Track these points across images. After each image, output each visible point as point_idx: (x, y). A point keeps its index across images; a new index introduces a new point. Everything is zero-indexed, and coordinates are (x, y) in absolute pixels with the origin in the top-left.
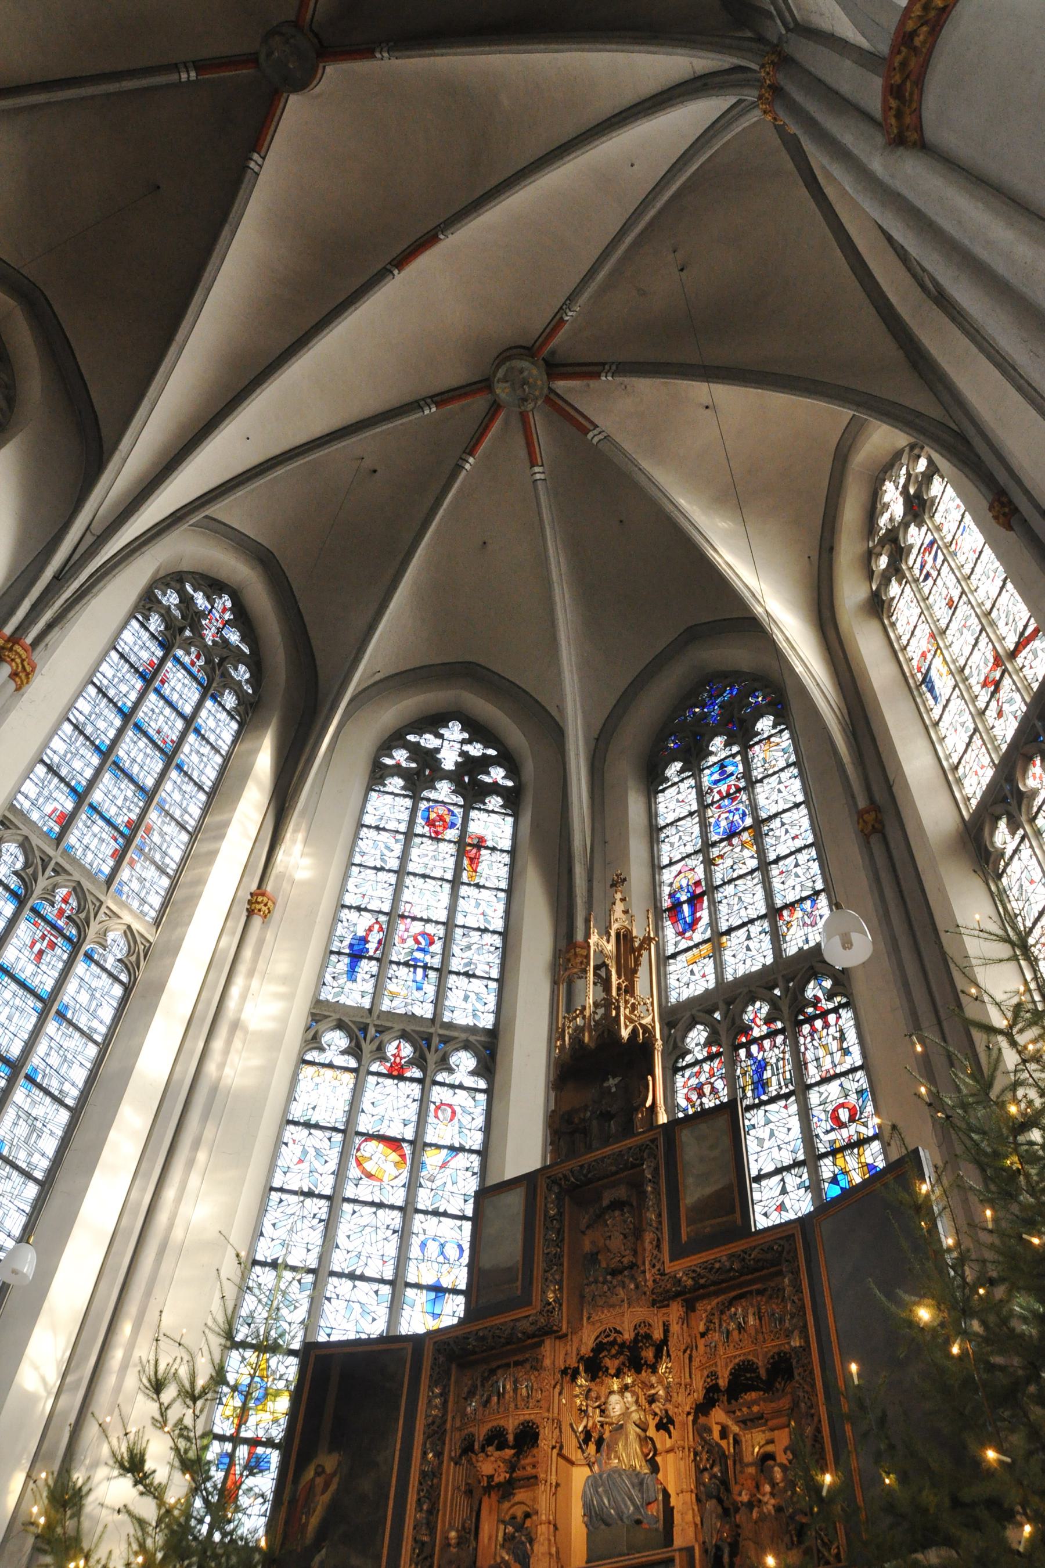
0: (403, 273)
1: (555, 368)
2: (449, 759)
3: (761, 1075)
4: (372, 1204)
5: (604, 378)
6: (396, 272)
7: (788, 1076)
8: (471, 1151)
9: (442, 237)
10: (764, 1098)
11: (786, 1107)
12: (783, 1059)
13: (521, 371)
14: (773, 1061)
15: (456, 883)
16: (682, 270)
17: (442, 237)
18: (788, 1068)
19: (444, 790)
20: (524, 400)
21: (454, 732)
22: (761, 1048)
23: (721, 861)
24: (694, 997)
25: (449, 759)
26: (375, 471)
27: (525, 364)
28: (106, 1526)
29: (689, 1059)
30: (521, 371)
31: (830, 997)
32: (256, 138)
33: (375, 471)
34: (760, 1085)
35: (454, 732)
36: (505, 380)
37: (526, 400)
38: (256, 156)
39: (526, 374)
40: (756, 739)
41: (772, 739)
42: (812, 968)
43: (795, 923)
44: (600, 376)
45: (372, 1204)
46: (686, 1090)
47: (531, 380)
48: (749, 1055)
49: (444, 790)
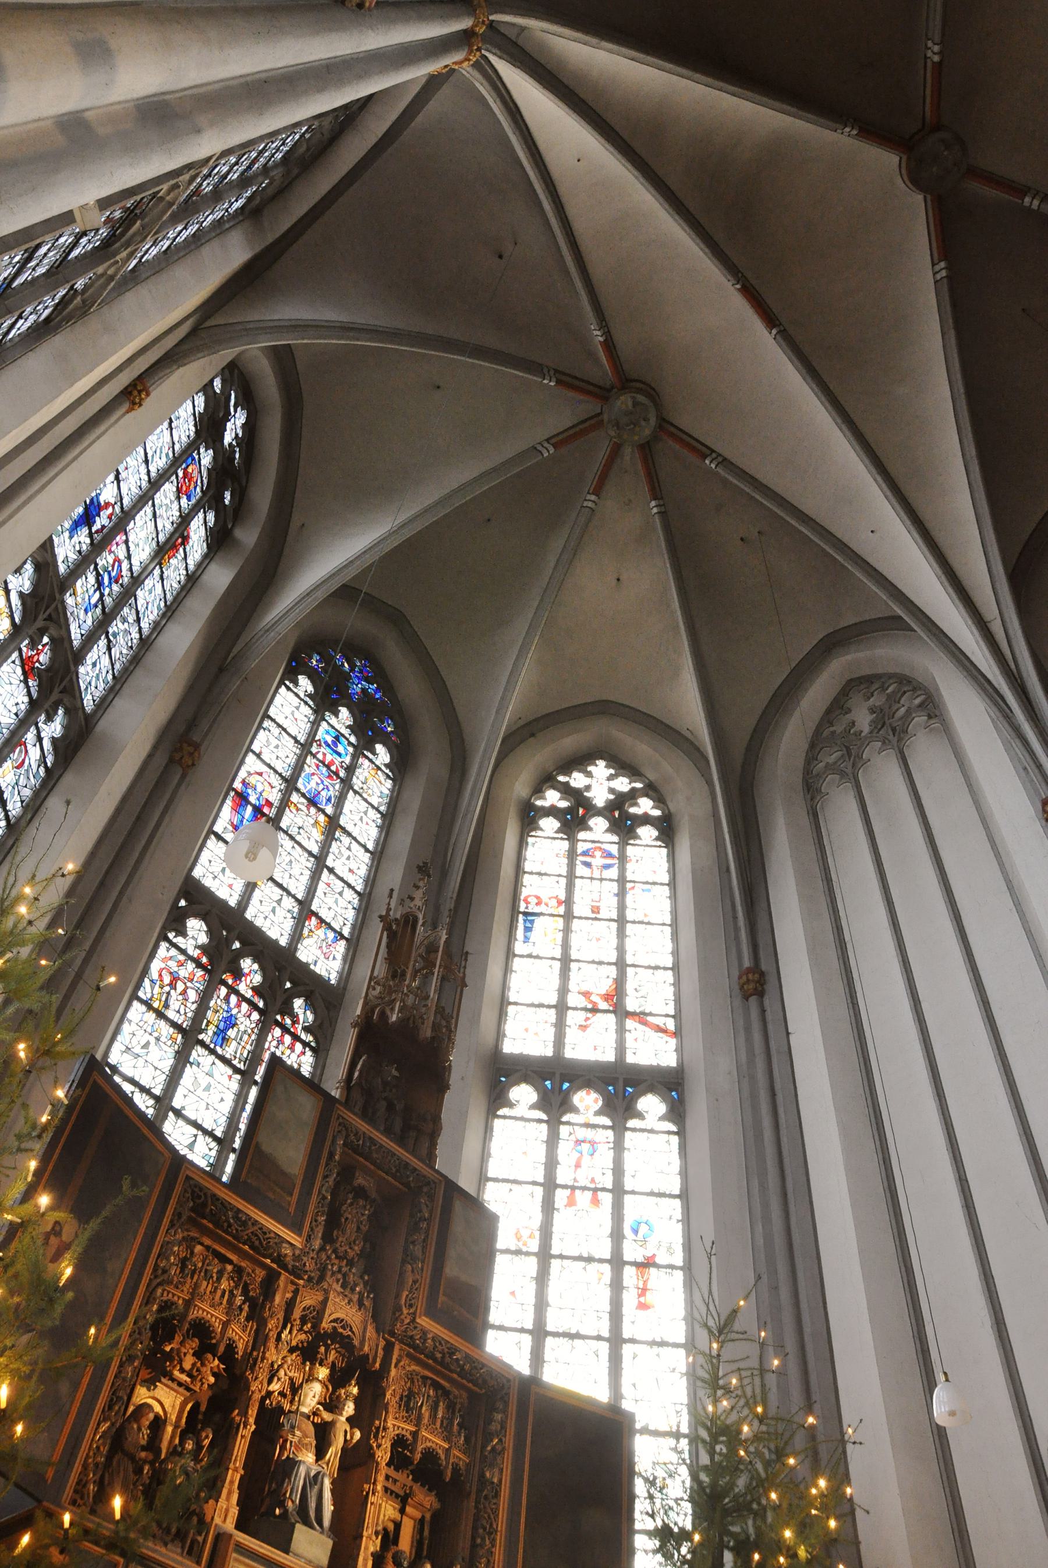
0: (736, 293)
1: (646, 450)
2: (600, 796)
3: (226, 1029)
4: (580, 1258)
5: (653, 504)
6: (738, 286)
7: (245, 1055)
8: (601, 1261)
9: (774, 331)
10: (219, 1050)
11: (230, 1077)
12: (249, 1036)
13: (646, 420)
14: (242, 1028)
15: (621, 964)
16: (742, 539)
17: (774, 331)
18: (249, 1047)
19: (599, 825)
20: (617, 425)
21: (600, 769)
22: (239, 1005)
23: (294, 811)
24: (264, 933)
25: (600, 796)
26: (501, 257)
27: (653, 421)
28: (8, 1176)
29: (179, 941)
30: (646, 420)
31: (306, 1029)
32: (872, 131)
33: (501, 257)
34: (222, 1035)
35: (600, 769)
36: (635, 404)
37: (618, 428)
38: (855, 132)
39: (643, 423)
40: (291, 686)
41: (379, 772)
42: (312, 992)
43: (315, 937)
44: (655, 499)
45: (580, 1258)
46: (163, 966)
47: (637, 429)
48: (227, 999)
49: (599, 825)
